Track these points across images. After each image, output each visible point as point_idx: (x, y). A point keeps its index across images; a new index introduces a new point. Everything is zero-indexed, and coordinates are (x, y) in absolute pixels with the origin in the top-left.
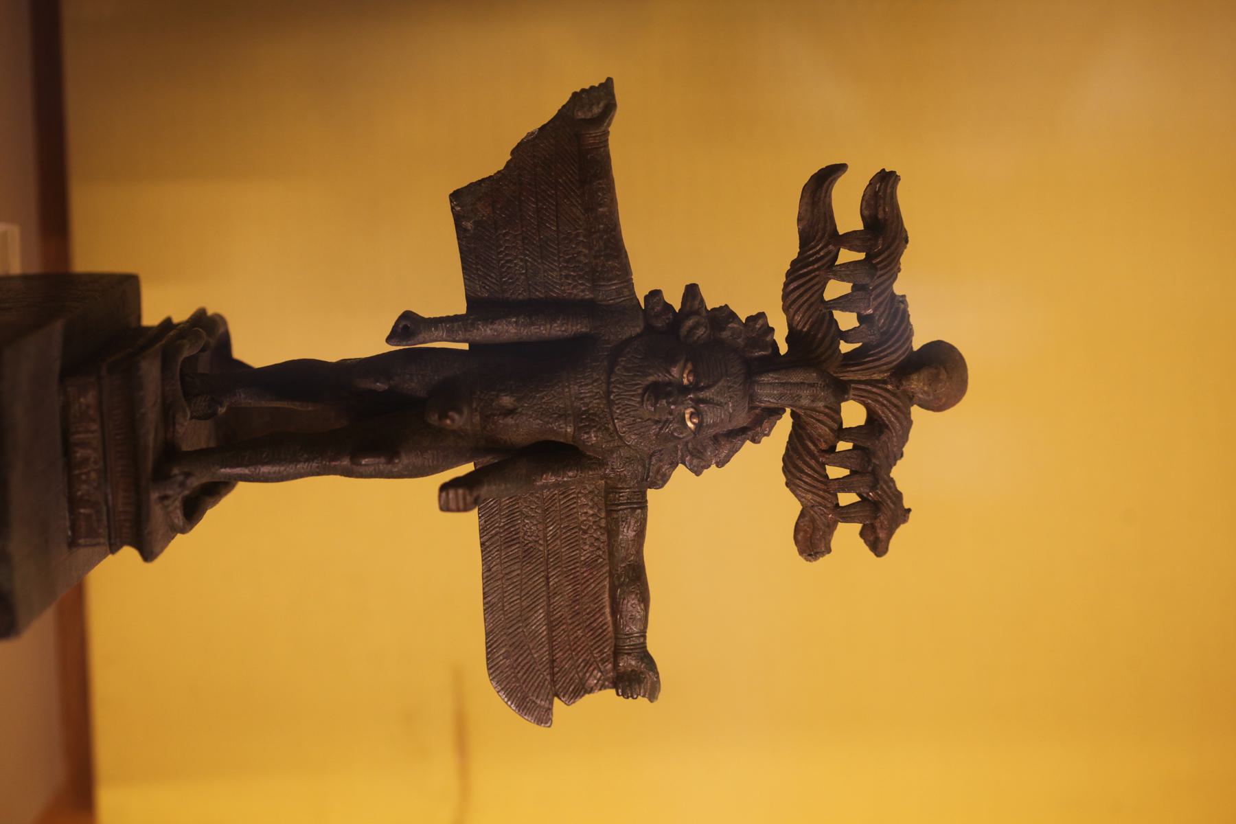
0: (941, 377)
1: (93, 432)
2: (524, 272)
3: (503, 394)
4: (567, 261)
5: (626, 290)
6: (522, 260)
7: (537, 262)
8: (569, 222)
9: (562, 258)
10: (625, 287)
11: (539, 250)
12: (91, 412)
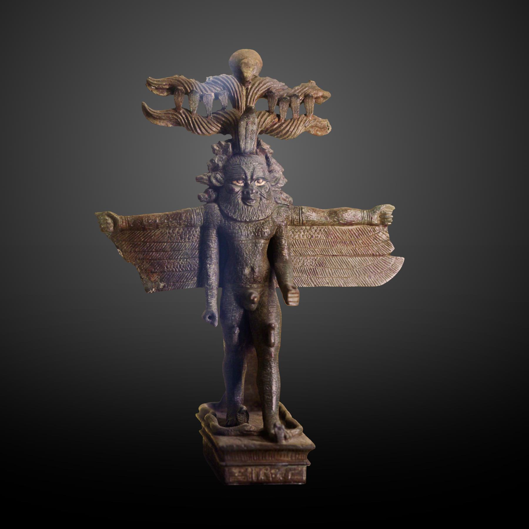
0: (246, 62)
1: (252, 470)
2: (185, 259)
3: (244, 273)
4: (182, 238)
5: (197, 211)
6: (180, 260)
7: (181, 253)
8: (162, 236)
9: (180, 241)
10: (196, 211)
11: (176, 252)
12: (242, 470)
